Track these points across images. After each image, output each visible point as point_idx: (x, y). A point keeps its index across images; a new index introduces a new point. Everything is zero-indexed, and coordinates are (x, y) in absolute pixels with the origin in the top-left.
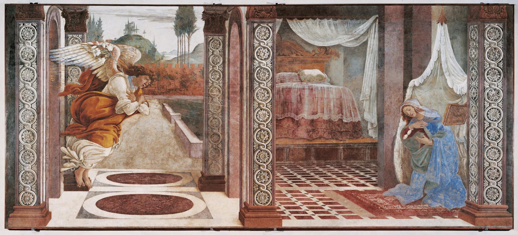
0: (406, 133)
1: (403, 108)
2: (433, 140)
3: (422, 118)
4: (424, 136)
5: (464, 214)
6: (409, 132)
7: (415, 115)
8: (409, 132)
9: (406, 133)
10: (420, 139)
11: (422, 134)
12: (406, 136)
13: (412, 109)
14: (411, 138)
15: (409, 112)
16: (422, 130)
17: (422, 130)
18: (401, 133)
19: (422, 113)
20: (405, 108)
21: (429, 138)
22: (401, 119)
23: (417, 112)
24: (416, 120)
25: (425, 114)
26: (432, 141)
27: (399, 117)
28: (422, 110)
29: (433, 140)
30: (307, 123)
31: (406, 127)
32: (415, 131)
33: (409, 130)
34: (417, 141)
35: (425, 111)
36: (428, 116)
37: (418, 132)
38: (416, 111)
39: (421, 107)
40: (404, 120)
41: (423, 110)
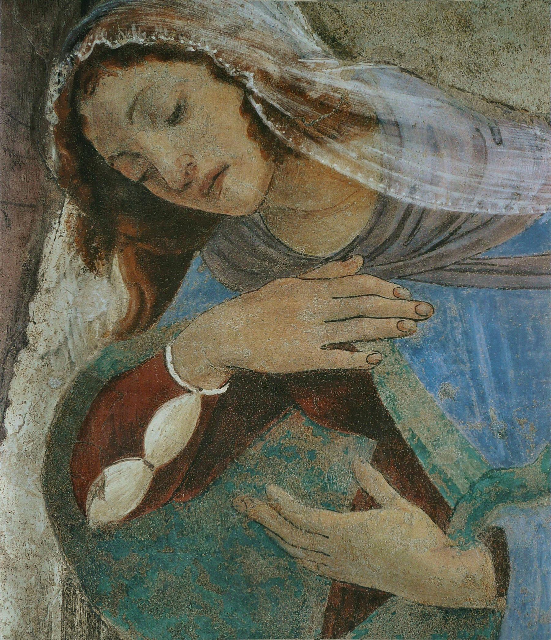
0: (132, 447)
1: (83, 81)
2: (498, 544)
3: (351, 224)
4: (378, 484)
5: (321, 263)
6: (168, 429)
7: (245, 186)
8: (168, 429)
9: (132, 447)
10: (324, 518)
11: (353, 458)
12: (122, 485)
13: (218, 118)
14: (201, 511)
15: (164, 151)
16: (350, 402)
17: (350, 402)
18: (56, 439)
19: (341, 159)
20: (115, 90)
21: (437, 508)
22: (58, 248)
23: (275, 151)
24: (260, 256)
25: (388, 171)
26: (478, 561)
27: (35, 214)
28: (345, 119)
29: (498, 544)
30: (171, 63)
31: (127, 355)
32: (252, 402)
33: (168, 390)
34: (273, 544)
35: (396, 129)
36: (437, 200)
37: (293, 429)
38: (258, 131)
39: (328, 76)
40: (92, 250)
41: (368, 122)
